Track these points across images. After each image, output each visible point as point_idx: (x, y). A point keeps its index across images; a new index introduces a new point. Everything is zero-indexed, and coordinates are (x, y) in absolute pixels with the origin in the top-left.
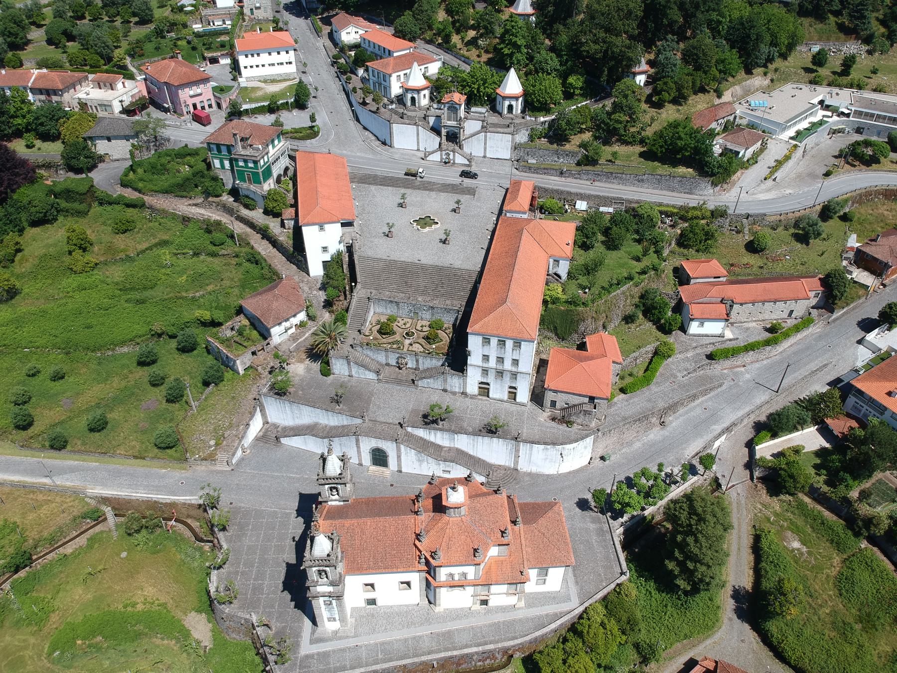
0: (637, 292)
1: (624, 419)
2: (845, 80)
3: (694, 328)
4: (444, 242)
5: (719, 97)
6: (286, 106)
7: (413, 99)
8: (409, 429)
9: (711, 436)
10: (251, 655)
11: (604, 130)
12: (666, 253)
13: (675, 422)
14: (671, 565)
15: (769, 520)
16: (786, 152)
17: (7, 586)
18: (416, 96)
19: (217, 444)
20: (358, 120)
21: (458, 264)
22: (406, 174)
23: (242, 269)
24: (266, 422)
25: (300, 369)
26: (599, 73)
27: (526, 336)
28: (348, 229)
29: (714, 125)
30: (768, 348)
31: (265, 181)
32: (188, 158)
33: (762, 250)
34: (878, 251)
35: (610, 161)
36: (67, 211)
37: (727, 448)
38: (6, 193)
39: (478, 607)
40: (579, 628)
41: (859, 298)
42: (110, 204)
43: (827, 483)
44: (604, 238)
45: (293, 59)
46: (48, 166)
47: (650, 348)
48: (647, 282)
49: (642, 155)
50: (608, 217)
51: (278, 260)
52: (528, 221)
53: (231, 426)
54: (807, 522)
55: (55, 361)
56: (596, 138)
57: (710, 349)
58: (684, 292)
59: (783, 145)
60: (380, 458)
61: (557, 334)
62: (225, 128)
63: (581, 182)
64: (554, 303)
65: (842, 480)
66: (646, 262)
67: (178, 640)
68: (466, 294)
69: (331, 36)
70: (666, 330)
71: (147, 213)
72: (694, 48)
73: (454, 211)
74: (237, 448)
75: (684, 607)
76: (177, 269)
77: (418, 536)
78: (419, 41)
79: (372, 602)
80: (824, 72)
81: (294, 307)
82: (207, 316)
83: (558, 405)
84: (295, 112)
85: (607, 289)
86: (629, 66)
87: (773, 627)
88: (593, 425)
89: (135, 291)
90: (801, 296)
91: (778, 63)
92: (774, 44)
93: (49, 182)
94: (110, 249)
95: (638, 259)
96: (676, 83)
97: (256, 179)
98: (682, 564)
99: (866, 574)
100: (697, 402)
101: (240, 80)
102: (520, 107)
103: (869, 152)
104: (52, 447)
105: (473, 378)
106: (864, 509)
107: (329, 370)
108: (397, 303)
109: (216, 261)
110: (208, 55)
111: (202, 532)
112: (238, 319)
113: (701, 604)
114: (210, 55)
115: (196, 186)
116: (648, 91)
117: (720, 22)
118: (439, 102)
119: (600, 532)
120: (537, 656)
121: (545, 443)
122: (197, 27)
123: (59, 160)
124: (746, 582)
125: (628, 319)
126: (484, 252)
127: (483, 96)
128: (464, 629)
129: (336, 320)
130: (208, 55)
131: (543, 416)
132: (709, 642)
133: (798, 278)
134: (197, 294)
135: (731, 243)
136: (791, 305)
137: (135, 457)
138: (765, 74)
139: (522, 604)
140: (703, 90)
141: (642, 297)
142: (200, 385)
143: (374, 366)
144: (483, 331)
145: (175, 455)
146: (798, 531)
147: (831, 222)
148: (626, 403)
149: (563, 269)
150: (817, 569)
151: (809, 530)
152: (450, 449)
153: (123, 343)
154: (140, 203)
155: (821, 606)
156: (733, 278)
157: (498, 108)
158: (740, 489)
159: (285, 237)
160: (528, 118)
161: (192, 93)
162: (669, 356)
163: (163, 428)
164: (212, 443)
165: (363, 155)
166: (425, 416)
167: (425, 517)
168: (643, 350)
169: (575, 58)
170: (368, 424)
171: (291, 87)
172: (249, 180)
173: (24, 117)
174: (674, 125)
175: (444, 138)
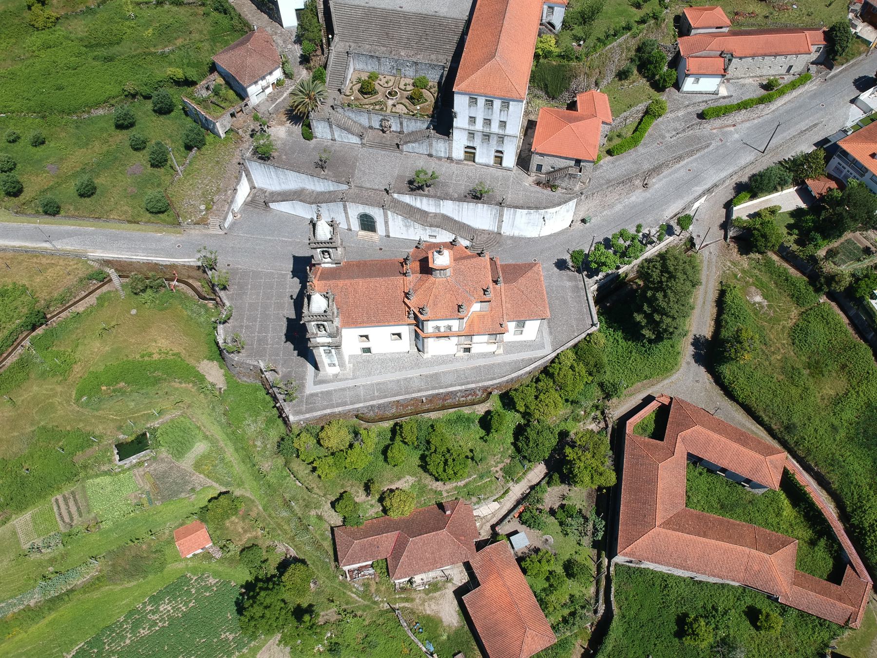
0: (633, 44)
1: (608, 181)
3: (689, 85)
8: (396, 196)
9: (691, 198)
10: (262, 394)
13: (658, 184)
14: (639, 317)
15: (735, 276)
17: (27, 343)
19: (207, 209)
21: (443, 11)
23: (210, 20)
24: (253, 187)
25: (281, 132)
27: (515, 95)
30: (761, 106)
37: (706, 209)
39: (461, 354)
40: (551, 370)
41: (860, 54)
43: (797, 242)
47: (642, 107)
48: (645, 33)
53: (218, 191)
55: (31, 127)
57: (702, 108)
60: (368, 223)
61: (547, 93)
64: (546, 57)
65: (813, 239)
67: (195, 384)
68: (452, 48)
70: (658, 86)
74: (227, 213)
75: (648, 353)
77: (407, 295)
79: (367, 350)
82: (179, 74)
83: (544, 170)
87: (727, 370)
88: (577, 188)
90: (802, 51)
98: (649, 317)
99: (821, 326)
100: (682, 163)
106: (829, 267)
107: (311, 133)
108: (379, 59)
111: (205, 291)
119: (576, 289)
120: (513, 393)
121: (529, 208)
124: (707, 331)
125: (622, 75)
129: (315, 78)
131: (528, 180)
132: (666, 382)
133: (802, 30)
134: (167, 50)
136: (792, 60)
139: (501, 351)
141: (639, 50)
142: (182, 149)
143: (356, 129)
144: (470, 90)
145: (167, 219)
146: (761, 286)
148: (611, 166)
151: (773, 286)
152: (436, 215)
153: (97, 105)
155: (773, 353)
156: (737, 29)
158: (712, 248)
162: (660, 116)
163: (151, 192)
164: (203, 207)
166: (411, 182)
167: (413, 278)
170: (354, 190)
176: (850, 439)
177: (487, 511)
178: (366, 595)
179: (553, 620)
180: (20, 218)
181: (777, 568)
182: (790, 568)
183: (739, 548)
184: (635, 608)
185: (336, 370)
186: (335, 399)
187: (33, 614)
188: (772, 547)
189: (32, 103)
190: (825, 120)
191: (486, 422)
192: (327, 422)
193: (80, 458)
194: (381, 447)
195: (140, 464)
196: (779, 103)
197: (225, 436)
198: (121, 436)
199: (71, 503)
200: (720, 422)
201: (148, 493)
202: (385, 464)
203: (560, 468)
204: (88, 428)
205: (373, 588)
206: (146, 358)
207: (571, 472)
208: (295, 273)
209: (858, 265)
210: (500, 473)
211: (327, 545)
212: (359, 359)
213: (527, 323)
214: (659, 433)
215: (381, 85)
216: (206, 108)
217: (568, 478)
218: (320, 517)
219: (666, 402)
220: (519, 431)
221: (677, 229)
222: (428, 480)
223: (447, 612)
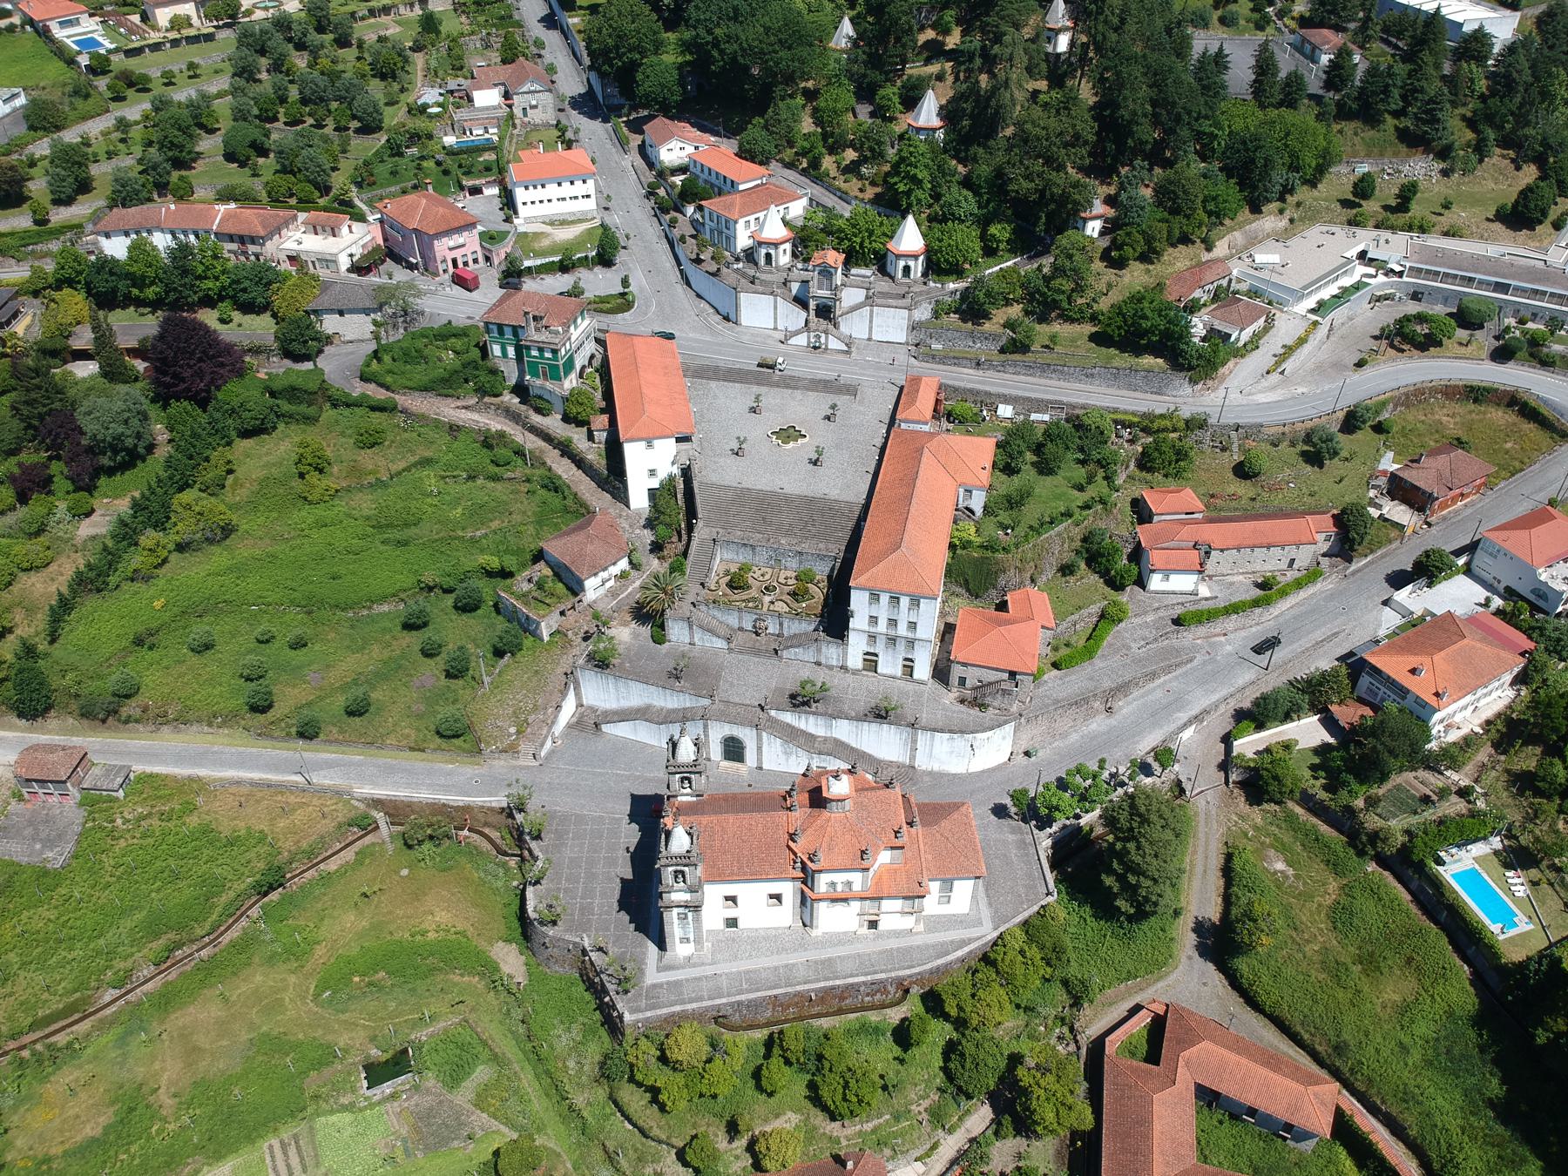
0: (1078, 533)
1: (1057, 701)
2: (1402, 219)
3: (1156, 582)
4: (815, 463)
5: (1209, 249)
6: (584, 262)
7: (768, 256)
8: (773, 713)
9: (1173, 727)
11: (1039, 303)
12: (1119, 481)
13: (1126, 708)
14: (1109, 881)
15: (1246, 835)
16: (1301, 332)
17: (255, 912)
18: (772, 252)
19: (518, 732)
20: (688, 284)
21: (834, 493)
22: (759, 365)
23: (537, 499)
25: (625, 634)
26: (1037, 221)
27: (926, 592)
29: (1197, 294)
30: (1258, 611)
31: (566, 375)
32: (453, 340)
33: (1256, 475)
34: (1419, 478)
35: (1047, 347)
36: (291, 417)
38: (208, 391)
39: (865, 930)
40: (992, 955)
41: (1390, 542)
42: (348, 406)
43: (1325, 788)
44: (1035, 458)
45: (592, 192)
46: (256, 351)
47: (1095, 609)
48: (1093, 520)
49: (1093, 338)
50: (1040, 429)
51: (585, 487)
52: (931, 435)
53: (535, 708)
54: (1296, 838)
55: (294, 623)
56: (1027, 313)
57: (1179, 611)
58: (1144, 533)
60: (734, 750)
61: (968, 590)
62: (510, 302)
63: (1007, 376)
64: (964, 548)
65: (1344, 784)
66: (1091, 492)
67: (482, 975)
69: (642, 149)
70: (1116, 584)
71: (400, 419)
72: (1171, 183)
73: (828, 418)
75: (1129, 937)
76: (447, 498)
77: (792, 837)
78: (774, 164)
80: (1371, 207)
81: (614, 551)
82: (495, 563)
83: (968, 684)
84: (598, 269)
85: (1036, 530)
86: (1076, 212)
87: (1242, 965)
88: (1014, 708)
89: (393, 528)
90: (1304, 540)
91: (1303, 193)
92: (1295, 168)
93: (262, 375)
94: (355, 470)
95: (1081, 488)
96: (1143, 233)
97: (554, 374)
98: (1121, 879)
99: (1371, 904)
100: (1158, 682)
101: (516, 221)
102: (920, 269)
103: (1421, 329)
104: (301, 735)
105: (857, 645)
106: (1372, 822)
108: (753, 547)
109: (499, 486)
110: (468, 182)
111: (507, 843)
112: (537, 567)
113: (1149, 934)
114: (470, 183)
115: (466, 381)
116: (1105, 243)
117: (1213, 137)
118: (806, 260)
119: (1022, 844)
121: (951, 731)
122: (450, 140)
123: (270, 341)
124: (1213, 912)
125: (1066, 570)
126: (870, 477)
127: (868, 253)
128: (848, 957)
129: (672, 570)
130: (468, 182)
131: (949, 697)
132: (1160, 985)
133: (1303, 514)
134: (478, 533)
135: (1213, 465)
136: (1291, 552)
137: (412, 749)
138: (1281, 212)
139: (921, 928)
140: (1185, 240)
141: (1085, 540)
142: (489, 655)
143: (722, 631)
144: (871, 584)
145: (466, 746)
146: (1283, 849)
147: (1359, 435)
149: (977, 502)
150: (1306, 896)
151: (1299, 848)
152: (826, 739)
153: (383, 599)
154: (390, 405)
155: (1308, 941)
156: (1214, 514)
157: (890, 269)
158: (1210, 795)
159: (594, 453)
160: (932, 284)
161: (452, 244)
162: (1120, 621)
163: (445, 711)
164: (513, 730)
165: (698, 336)
166: (793, 697)
167: (800, 814)
168: (1085, 612)
169: (997, 197)
171: (590, 231)
172: (545, 374)
173: (217, 279)
174: (1137, 299)
175: (812, 313)
176: (1429, 1063)
180: (261, 743)
186: (687, 992)
189: (296, 595)
191: (903, 1036)
192: (676, 1021)
193: (313, 1082)
194: (751, 1068)
195: (394, 1096)
196: (1283, 607)
197: (521, 1056)
198: (374, 1052)
199: (292, 1151)
200: (1238, 1039)
201: (404, 1140)
202: (757, 1094)
203: (1014, 1111)
204: (330, 1038)
206: (418, 938)
207: (1028, 1109)
208: (633, 817)
209: (1413, 821)
210: (925, 1116)
212: (721, 937)
213: (956, 883)
214: (1153, 1057)
215: (755, 578)
217: (1025, 1125)
219: (1161, 1010)
220: (950, 1049)
221: (1156, 766)
222: (819, 1118)
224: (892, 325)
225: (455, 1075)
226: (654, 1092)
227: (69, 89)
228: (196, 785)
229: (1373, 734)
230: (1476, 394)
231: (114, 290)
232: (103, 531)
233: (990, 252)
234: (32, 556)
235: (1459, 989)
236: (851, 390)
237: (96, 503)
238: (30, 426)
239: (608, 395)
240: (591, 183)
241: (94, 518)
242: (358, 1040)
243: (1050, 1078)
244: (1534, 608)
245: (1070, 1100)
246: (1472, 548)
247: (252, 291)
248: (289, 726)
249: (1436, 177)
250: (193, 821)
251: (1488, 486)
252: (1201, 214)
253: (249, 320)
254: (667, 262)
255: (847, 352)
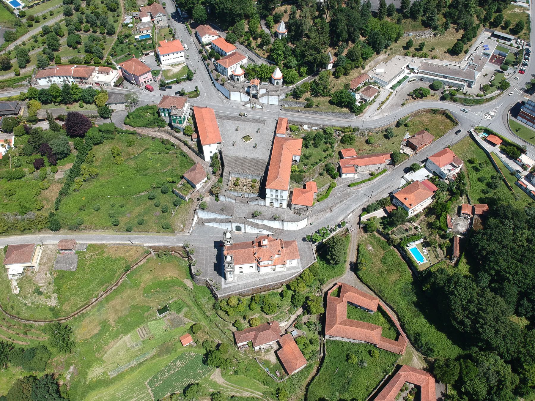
0: (324, 164)
1: (318, 211)
2: (420, 53)
3: (344, 176)
5: (363, 69)
7: (238, 79)
13: (335, 210)
14: (328, 257)
17: (124, 276)
20: (214, 86)
21: (260, 157)
25: (208, 199)
28: (219, 145)
34: (414, 141)
37: (351, 218)
39: (272, 272)
43: (383, 228)
45: (183, 56)
46: (93, 117)
47: (328, 185)
49: (331, 102)
57: (349, 183)
59: (387, 92)
66: (327, 152)
67: (182, 287)
68: (264, 169)
70: (333, 177)
75: (333, 268)
77: (255, 254)
78: (237, 44)
79: (241, 272)
80: (412, 49)
82: (171, 179)
84: (188, 82)
85: (313, 165)
87: (360, 273)
89: (141, 170)
91: (393, 45)
94: (128, 154)
95: (325, 151)
98: (331, 257)
105: (268, 201)
111: (184, 254)
114: (146, 53)
119: (309, 248)
120: (290, 284)
123: (97, 114)
124: (354, 260)
125: (321, 174)
127: (265, 77)
130: (145, 52)
131: (291, 212)
136: (379, 165)
138: (386, 52)
140: (357, 67)
141: (326, 166)
146: (371, 244)
147: (400, 128)
149: (298, 159)
151: (375, 243)
153: (143, 192)
156: (360, 155)
164: (182, 226)
166: (253, 215)
167: (256, 248)
170: (234, 218)
177: (284, 325)
178: (245, 354)
179: (307, 358)
180: (117, 233)
181: (375, 335)
182: (380, 336)
183: (363, 329)
184: (333, 353)
185: (232, 279)
187: (132, 369)
188: (373, 329)
190: (392, 185)
191: (282, 295)
193: (146, 314)
195: (165, 316)
203: (307, 309)
205: (248, 352)
208: (215, 247)
209: (403, 236)
210: (287, 312)
211: (232, 338)
214: (338, 296)
216: (181, 191)
217: (309, 312)
218: (229, 329)
220: (293, 297)
223: (272, 358)
224: (274, 100)
225: (179, 310)
226: (227, 312)
227: (14, 23)
228: (103, 246)
229: (394, 213)
230: (434, 111)
231: (47, 99)
232: (62, 177)
233: (301, 75)
234: (45, 186)
235: (409, 277)
236: (263, 122)
237: (57, 167)
238: (35, 147)
239: (196, 126)
240: (183, 53)
241: (59, 172)
242: (156, 305)
243: (314, 303)
244: (440, 177)
245: (319, 307)
246: (425, 161)
247: (88, 97)
248: (124, 228)
249: (432, 36)
250: (105, 255)
251: (433, 141)
252: (361, 59)
253: (88, 106)
254: (208, 78)
255: (262, 109)
